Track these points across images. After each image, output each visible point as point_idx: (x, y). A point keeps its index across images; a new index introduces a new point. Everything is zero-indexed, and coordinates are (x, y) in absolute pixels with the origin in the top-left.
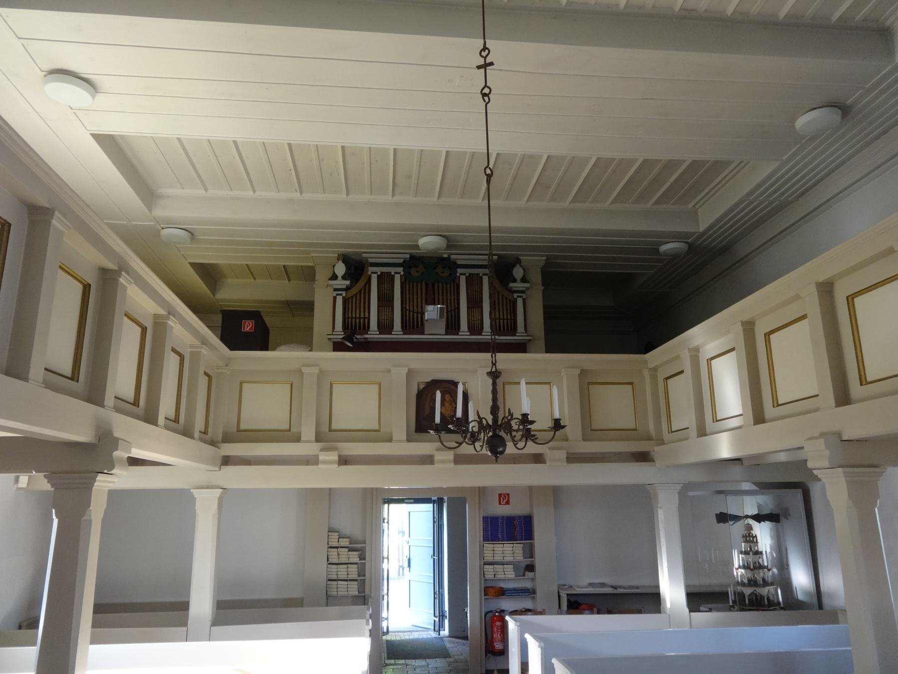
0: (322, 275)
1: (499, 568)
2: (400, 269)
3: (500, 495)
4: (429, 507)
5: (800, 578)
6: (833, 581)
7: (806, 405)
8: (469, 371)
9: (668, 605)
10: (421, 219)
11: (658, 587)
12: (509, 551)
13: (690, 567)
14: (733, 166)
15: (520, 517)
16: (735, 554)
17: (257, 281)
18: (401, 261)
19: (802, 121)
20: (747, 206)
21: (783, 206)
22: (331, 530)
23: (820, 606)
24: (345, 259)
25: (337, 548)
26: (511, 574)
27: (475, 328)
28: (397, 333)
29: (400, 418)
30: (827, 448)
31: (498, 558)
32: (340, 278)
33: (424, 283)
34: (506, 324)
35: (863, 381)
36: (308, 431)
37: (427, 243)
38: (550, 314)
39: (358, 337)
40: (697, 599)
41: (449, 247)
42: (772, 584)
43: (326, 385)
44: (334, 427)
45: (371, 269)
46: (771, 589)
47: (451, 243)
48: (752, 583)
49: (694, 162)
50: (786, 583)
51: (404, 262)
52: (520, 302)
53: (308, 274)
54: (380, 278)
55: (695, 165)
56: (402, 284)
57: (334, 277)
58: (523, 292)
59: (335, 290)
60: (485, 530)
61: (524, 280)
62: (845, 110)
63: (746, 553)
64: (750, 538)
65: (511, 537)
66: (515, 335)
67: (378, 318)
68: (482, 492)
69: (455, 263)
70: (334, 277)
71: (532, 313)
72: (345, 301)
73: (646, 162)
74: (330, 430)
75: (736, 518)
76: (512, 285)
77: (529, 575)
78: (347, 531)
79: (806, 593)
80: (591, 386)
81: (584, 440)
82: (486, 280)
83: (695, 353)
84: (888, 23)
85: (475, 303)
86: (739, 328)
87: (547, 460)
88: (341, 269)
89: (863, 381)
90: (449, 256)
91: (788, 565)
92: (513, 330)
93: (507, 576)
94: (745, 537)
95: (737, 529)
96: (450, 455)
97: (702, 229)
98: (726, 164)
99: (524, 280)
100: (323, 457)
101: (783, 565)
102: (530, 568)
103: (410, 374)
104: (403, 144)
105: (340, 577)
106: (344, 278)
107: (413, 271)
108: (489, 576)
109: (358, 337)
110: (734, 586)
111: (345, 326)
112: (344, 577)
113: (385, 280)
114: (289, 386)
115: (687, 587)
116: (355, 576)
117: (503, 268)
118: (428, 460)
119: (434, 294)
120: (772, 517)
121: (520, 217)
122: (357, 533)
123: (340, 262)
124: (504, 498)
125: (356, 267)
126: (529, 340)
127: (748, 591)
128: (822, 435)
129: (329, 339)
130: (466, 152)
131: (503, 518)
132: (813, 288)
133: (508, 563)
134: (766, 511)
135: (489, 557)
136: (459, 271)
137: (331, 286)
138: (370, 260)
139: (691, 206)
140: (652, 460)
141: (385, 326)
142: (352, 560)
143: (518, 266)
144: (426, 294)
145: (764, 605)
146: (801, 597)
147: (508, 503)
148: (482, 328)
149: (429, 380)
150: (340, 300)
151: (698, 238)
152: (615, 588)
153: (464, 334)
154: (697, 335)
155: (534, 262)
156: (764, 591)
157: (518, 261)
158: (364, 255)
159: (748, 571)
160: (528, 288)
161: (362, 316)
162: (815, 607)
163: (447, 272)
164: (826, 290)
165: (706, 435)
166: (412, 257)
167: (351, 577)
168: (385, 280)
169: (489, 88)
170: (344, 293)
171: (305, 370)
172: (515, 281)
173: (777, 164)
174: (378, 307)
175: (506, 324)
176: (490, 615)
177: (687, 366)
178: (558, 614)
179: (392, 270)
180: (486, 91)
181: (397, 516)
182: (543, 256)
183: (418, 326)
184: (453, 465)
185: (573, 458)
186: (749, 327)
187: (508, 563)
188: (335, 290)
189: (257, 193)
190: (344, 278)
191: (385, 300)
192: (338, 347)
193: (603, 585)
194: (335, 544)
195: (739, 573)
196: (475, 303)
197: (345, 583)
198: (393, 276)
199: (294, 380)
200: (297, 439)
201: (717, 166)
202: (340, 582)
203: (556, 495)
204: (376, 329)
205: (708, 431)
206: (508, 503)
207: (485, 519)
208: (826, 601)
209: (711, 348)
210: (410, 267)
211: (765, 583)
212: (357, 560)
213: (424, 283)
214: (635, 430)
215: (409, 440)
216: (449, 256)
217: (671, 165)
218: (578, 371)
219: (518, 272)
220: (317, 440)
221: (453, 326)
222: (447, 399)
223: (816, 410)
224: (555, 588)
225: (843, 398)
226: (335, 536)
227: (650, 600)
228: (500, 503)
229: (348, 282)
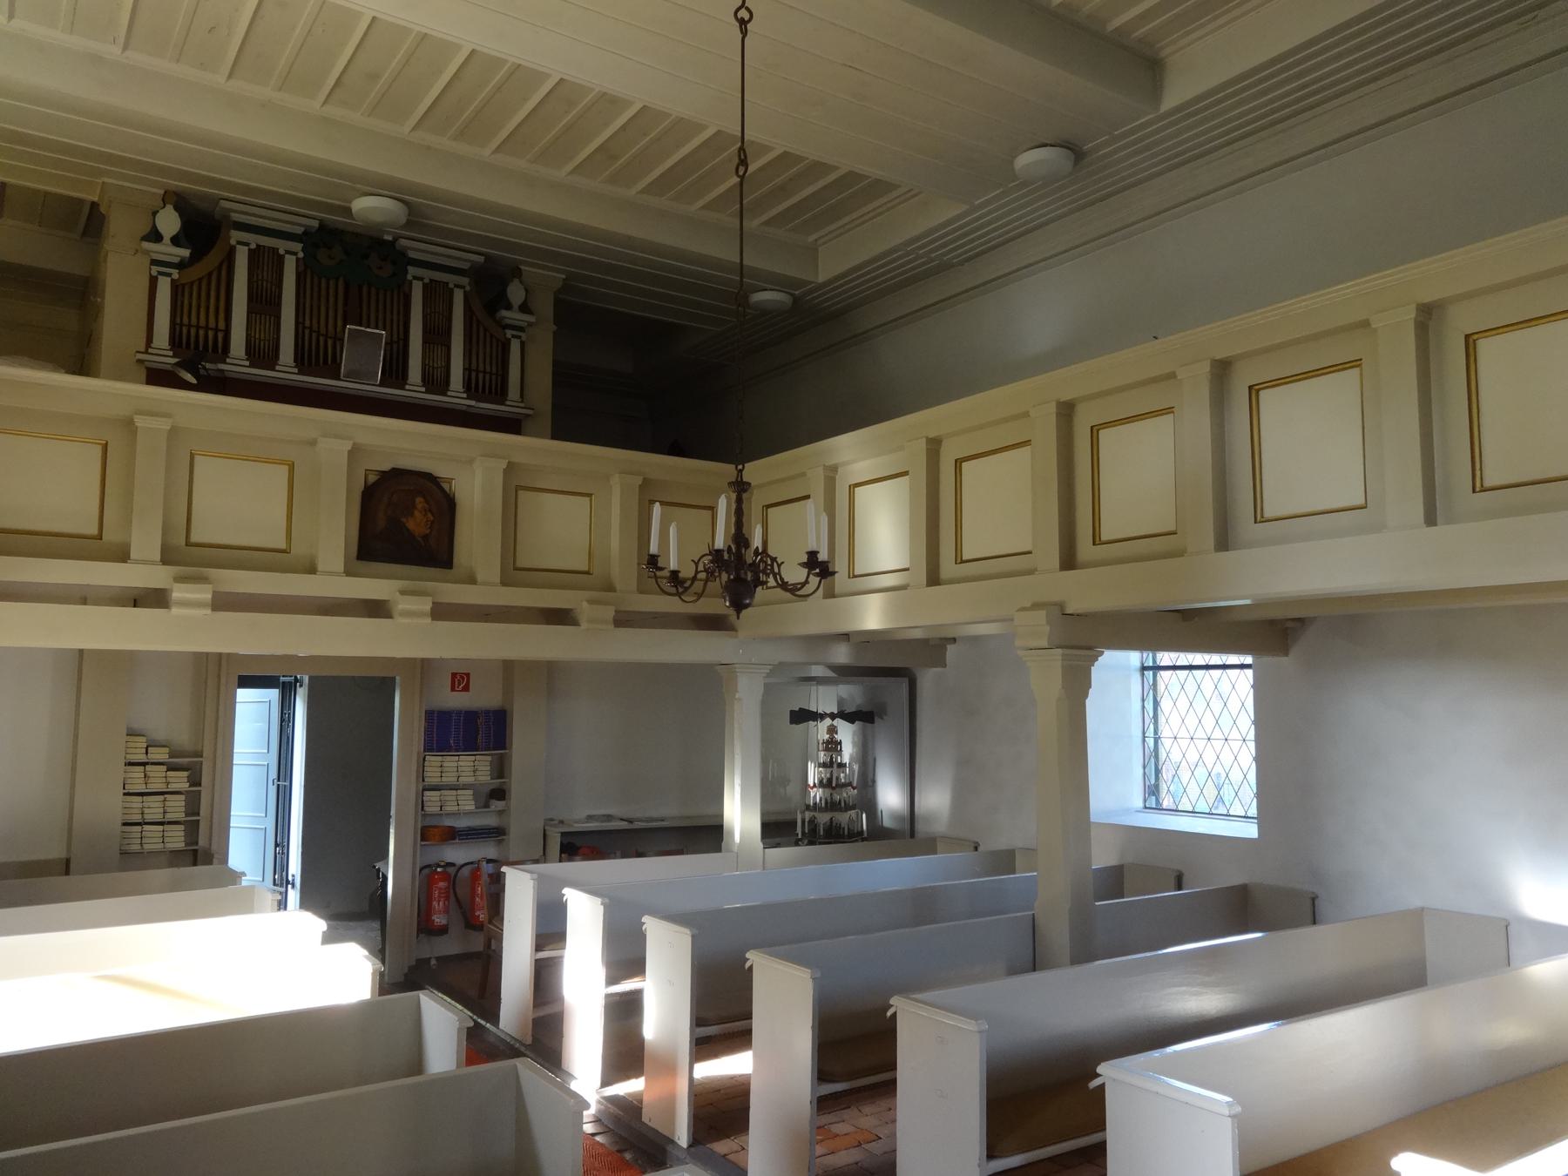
0: (121, 229)
1: (449, 795)
2: (298, 247)
3: (454, 675)
4: (273, 694)
5: (890, 797)
6: (936, 800)
7: (1009, 566)
8: (469, 463)
9: (737, 838)
10: (371, 161)
11: (722, 816)
12: (470, 768)
13: (771, 787)
14: (895, 194)
15: (487, 712)
16: (811, 767)
18: (299, 230)
19: (1026, 160)
20: (899, 258)
21: (942, 268)
22: (131, 733)
23: (912, 835)
24: (179, 201)
25: (144, 764)
26: (467, 802)
27: (436, 380)
28: (456, 395)
29: (332, 533)
30: (1048, 622)
31: (449, 779)
32: (167, 239)
33: (341, 282)
34: (488, 382)
35: (1096, 540)
36: (146, 542)
37: (369, 207)
38: (563, 376)
39: (208, 366)
40: (775, 830)
41: (409, 224)
42: (853, 808)
43: (183, 456)
44: (194, 538)
45: (236, 236)
46: (853, 813)
47: (416, 218)
48: (832, 806)
49: (851, 173)
50: (868, 802)
51: (305, 233)
52: (515, 347)
53: (89, 223)
54: (255, 255)
55: (852, 177)
59: (154, 262)
60: (428, 733)
62: (1076, 152)
63: (824, 765)
64: (833, 745)
65: (470, 746)
66: (503, 404)
67: (248, 335)
68: (424, 667)
69: (403, 254)
70: (155, 236)
71: (532, 369)
72: (176, 288)
73: (785, 155)
74: (188, 544)
75: (817, 716)
76: (504, 313)
77: (497, 805)
78: (160, 735)
79: (897, 817)
80: (521, 493)
81: (504, 583)
82: (459, 298)
83: (831, 474)
84: (1163, 54)
85: (437, 336)
86: (922, 445)
87: (395, 614)
88: (169, 222)
89: (1096, 540)
90: (395, 240)
91: (874, 781)
92: (500, 394)
93: (462, 808)
94: (827, 743)
95: (821, 730)
96: (204, 594)
97: (821, 279)
98: (888, 187)
99: (524, 308)
100: (179, 593)
101: (867, 784)
102: (499, 794)
103: (355, 453)
104: (491, 46)
105: (148, 818)
106: (175, 241)
108: (432, 808)
109: (208, 366)
110: (803, 812)
111: (175, 342)
112: (159, 818)
113: (265, 264)
114: (98, 450)
115: (763, 815)
116: (181, 816)
117: (491, 281)
118: (376, 609)
120: (860, 716)
121: (491, 184)
122: (183, 738)
123: (170, 208)
124: (461, 681)
125: (203, 226)
126: (528, 416)
127: (823, 818)
128: (1036, 606)
129: (140, 361)
130: (506, 61)
131: (459, 713)
132: (1052, 408)
133: (465, 787)
134: (850, 709)
135: (433, 777)
137: (147, 252)
138: (236, 217)
139: (811, 238)
140: (389, 616)
141: (263, 354)
142: (173, 787)
143: (516, 281)
144: (345, 304)
145: (843, 836)
146: (887, 823)
147: (466, 688)
148: (447, 382)
149: (386, 467)
150: (164, 287)
151: (811, 291)
152: (630, 821)
153: (414, 389)
154: (852, 452)
156: (843, 818)
157: (516, 272)
158: (224, 204)
159: (828, 791)
160: (530, 324)
161: (202, 323)
162: (906, 835)
164: (1066, 412)
165: (834, 596)
166: (323, 226)
167: (170, 817)
169: (748, 9)
170: (175, 274)
171: (140, 421)
172: (509, 307)
173: (965, 207)
174: (249, 312)
175: (488, 382)
176: (426, 871)
177: (818, 489)
179: (282, 245)
180: (743, 14)
181: (252, 711)
182: (558, 271)
183: (325, 362)
184: (429, 620)
185: (624, 620)
186: (934, 447)
187: (465, 787)
188: (154, 262)
189: (17, 23)
190: (175, 241)
191: (264, 303)
192: (157, 377)
193: (609, 818)
194: (142, 758)
195: (817, 795)
196: (437, 336)
197: (160, 828)
198: (451, 291)
199: (114, 444)
200: (122, 555)
201: (878, 188)
202: (146, 827)
203: (549, 674)
204: (460, 388)
205: (837, 591)
206: (466, 688)
207: (429, 715)
208: (920, 827)
209: (862, 468)
211: (848, 808)
212: (185, 786)
213: (341, 282)
214: (587, 573)
215: (349, 572)
216: (395, 240)
217: (819, 168)
218: (639, 480)
219: (516, 293)
220: (165, 561)
221: (395, 372)
222: (419, 506)
223: (1031, 572)
224: (540, 825)
225: (1069, 561)
226: (141, 743)
227: (709, 835)
228: (453, 689)
229: (186, 253)
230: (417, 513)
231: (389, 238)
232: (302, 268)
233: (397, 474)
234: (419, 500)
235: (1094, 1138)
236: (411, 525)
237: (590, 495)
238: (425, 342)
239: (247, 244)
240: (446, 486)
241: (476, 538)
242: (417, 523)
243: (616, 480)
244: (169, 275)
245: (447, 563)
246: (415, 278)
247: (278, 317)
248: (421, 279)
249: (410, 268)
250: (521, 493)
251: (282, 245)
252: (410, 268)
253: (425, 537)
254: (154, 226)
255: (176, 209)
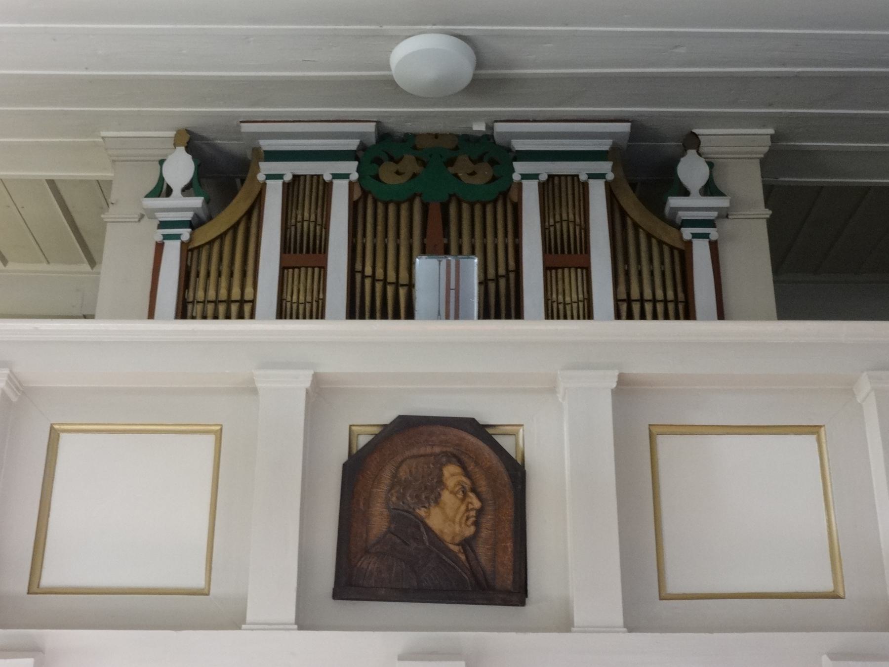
17: (11, 266)
18: (352, 145)
45: (266, 167)
51: (363, 147)
52: (701, 253)
54: (293, 190)
56: (354, 208)
57: (162, 190)
58: (710, 223)
59: (163, 225)
61: (710, 189)
69: (509, 149)
70: (162, 190)
72: (188, 252)
74: (34, 587)
76: (674, 202)
88: (180, 168)
99: (710, 189)
103: (320, 394)
106: (187, 190)
107: (387, 173)
113: (308, 196)
119: (446, 234)
123: (181, 150)
136: (520, 168)
137: (151, 213)
143: (692, 153)
144: (424, 234)
149: (387, 417)
150: (172, 254)
155: (737, 144)
157: (692, 141)
158: (246, 128)
160: (724, 214)
163: (485, 172)
168: (308, 196)
170: (185, 233)
172: (685, 192)
174: (283, 269)
178: (438, 319)
198: (585, 185)
210: (379, 162)
216: (490, 128)
219: (692, 171)
222: (451, 482)
229: (197, 202)
230: (446, 496)
231: (479, 127)
232: (357, 194)
233: (407, 427)
234: (452, 474)
235: (681, 315)
236: (436, 520)
237: (814, 430)
238: (547, 268)
239: (279, 177)
240: (506, 443)
241: (571, 534)
242: (448, 517)
243: (865, 387)
244: (177, 237)
245: (516, 593)
246: (525, 177)
247: (323, 268)
248: (534, 176)
249: (516, 165)
250: (665, 443)
251: (325, 170)
252: (516, 165)
253: (467, 544)
254: (161, 179)
255: (188, 150)
